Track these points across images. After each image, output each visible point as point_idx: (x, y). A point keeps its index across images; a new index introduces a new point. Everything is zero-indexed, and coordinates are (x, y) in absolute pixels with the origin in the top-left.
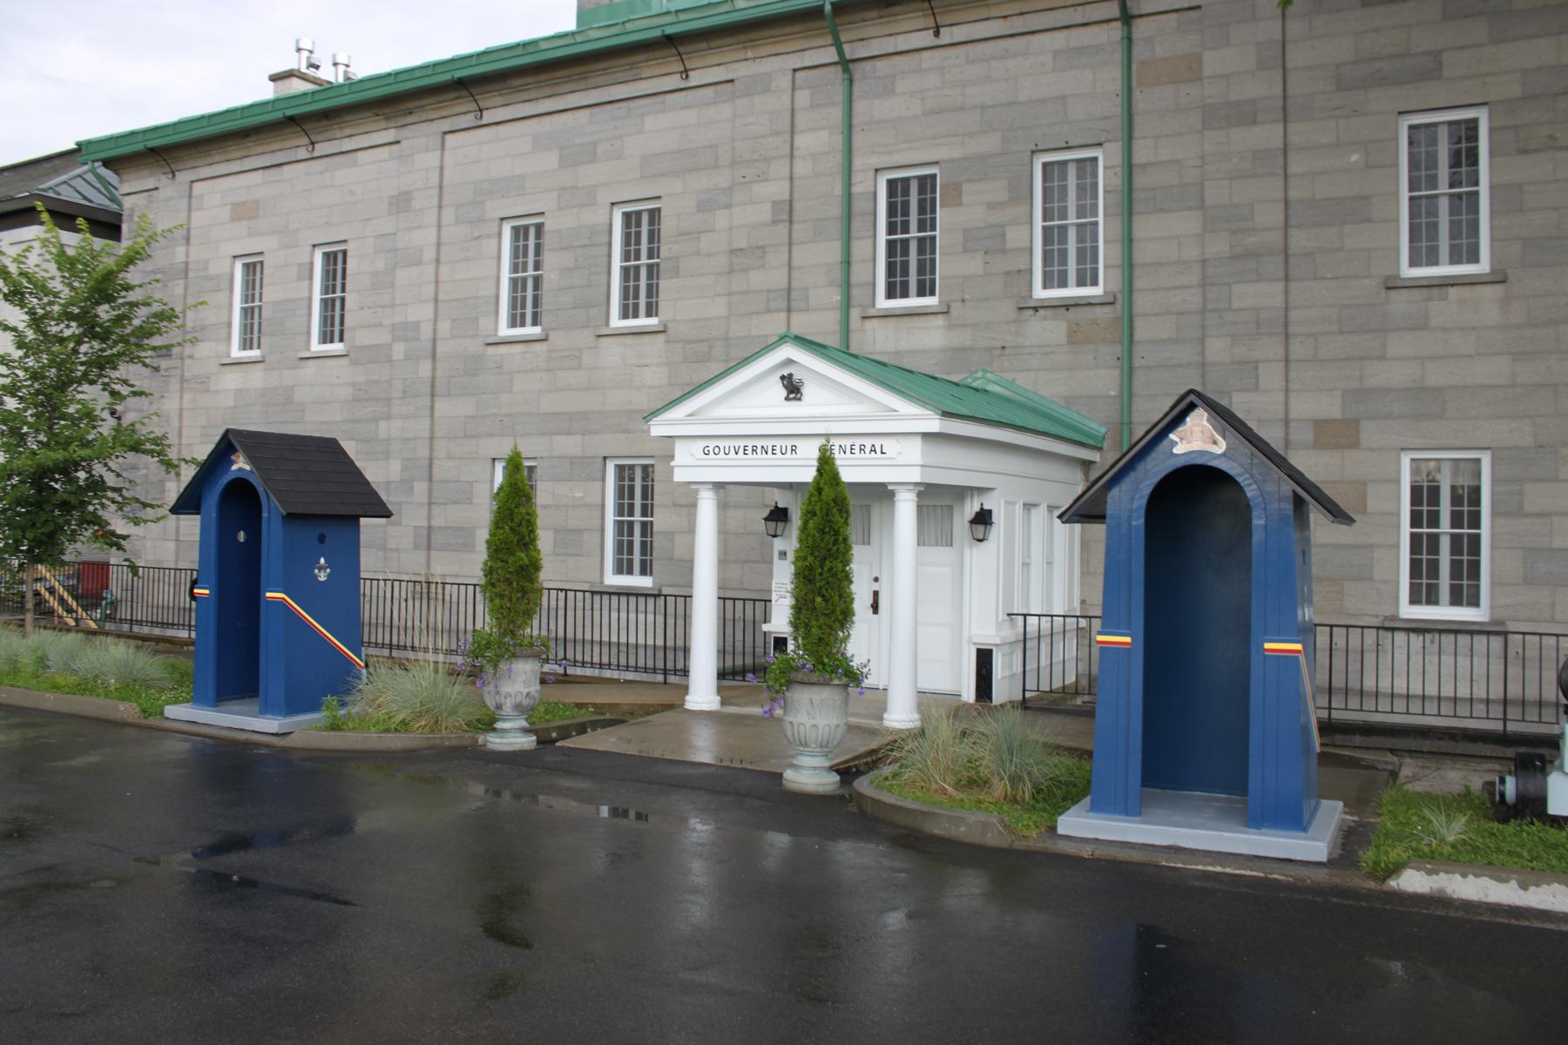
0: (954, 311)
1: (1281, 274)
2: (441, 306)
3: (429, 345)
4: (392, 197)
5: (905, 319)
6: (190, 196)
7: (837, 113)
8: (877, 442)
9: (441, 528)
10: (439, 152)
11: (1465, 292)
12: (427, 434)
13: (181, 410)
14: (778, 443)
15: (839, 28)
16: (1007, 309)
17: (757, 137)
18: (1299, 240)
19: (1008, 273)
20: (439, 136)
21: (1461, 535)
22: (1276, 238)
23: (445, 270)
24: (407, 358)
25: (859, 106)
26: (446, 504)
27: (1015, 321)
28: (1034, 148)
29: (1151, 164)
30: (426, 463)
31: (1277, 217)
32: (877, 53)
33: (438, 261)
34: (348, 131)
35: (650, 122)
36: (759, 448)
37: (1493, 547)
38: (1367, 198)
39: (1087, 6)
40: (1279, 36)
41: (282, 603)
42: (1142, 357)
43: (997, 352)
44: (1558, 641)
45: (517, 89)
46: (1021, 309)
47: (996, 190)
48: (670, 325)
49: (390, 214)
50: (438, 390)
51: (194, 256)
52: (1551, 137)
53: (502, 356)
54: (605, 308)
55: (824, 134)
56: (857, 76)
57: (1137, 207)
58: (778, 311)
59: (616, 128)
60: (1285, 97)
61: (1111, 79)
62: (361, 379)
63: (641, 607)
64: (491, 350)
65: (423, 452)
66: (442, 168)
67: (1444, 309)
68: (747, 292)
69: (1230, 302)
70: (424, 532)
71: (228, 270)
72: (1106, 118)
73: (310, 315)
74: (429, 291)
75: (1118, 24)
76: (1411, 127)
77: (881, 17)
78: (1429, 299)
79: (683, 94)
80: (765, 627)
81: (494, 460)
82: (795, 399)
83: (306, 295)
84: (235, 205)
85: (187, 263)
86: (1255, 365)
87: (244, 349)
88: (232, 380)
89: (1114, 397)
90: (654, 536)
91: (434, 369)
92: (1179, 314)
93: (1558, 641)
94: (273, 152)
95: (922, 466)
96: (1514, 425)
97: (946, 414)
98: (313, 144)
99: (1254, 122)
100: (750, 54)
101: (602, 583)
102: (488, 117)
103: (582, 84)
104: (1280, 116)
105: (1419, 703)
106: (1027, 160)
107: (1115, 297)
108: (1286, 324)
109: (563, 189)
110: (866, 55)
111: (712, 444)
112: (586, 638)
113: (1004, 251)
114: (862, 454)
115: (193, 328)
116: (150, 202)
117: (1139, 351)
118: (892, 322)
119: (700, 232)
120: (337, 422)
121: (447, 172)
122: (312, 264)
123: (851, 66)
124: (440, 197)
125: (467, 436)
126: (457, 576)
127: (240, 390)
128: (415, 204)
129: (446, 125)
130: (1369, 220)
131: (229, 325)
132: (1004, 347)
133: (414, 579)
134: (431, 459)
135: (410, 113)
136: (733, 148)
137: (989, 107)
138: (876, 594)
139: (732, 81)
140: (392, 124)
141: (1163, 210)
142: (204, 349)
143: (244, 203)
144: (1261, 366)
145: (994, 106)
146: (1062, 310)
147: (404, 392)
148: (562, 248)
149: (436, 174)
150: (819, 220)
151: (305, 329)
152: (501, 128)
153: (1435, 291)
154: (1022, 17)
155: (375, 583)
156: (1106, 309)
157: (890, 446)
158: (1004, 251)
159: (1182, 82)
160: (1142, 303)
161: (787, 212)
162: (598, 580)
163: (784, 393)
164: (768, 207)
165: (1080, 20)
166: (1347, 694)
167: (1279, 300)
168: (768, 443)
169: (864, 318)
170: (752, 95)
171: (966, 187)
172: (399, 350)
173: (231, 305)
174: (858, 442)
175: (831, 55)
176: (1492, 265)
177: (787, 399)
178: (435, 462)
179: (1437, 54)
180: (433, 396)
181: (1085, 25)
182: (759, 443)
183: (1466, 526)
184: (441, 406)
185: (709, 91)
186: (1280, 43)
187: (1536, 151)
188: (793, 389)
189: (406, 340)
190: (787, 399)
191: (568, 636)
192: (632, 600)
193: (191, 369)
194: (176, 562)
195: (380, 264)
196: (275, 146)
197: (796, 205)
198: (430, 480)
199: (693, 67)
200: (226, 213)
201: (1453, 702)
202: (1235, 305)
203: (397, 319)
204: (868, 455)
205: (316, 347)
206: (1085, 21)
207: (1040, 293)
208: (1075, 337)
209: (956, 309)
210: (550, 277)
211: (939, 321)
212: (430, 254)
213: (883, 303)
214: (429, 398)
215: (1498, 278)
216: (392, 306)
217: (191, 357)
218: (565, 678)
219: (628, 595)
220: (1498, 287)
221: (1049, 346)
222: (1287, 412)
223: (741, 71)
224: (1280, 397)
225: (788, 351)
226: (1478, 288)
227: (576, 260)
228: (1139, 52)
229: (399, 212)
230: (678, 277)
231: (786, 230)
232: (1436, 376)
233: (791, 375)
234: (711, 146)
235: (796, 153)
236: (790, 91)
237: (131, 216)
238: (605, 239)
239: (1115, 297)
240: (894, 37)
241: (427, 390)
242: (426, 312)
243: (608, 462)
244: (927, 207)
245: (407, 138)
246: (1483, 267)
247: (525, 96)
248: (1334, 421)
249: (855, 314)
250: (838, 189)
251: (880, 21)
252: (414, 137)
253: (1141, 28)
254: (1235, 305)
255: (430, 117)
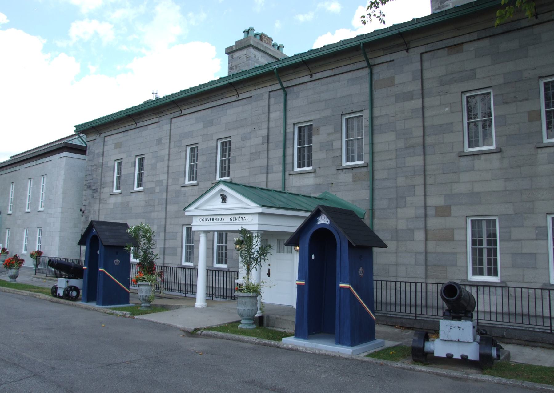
0: (317, 171)
1: (422, 153)
2: (170, 175)
3: (166, 188)
4: (157, 139)
5: (302, 175)
6: (104, 141)
7: (282, 106)
8: (246, 216)
9: (167, 248)
10: (169, 125)
11: (487, 157)
12: (164, 217)
13: (99, 209)
14: (219, 217)
15: (280, 77)
16: (333, 170)
17: (258, 115)
18: (429, 140)
19: (334, 157)
20: (170, 119)
21: (491, 249)
22: (420, 140)
23: (171, 162)
24: (159, 192)
25: (289, 102)
26: (169, 240)
27: (336, 174)
28: (342, 113)
29: (379, 116)
30: (164, 226)
31: (419, 132)
32: (294, 84)
33: (169, 160)
34: (146, 119)
35: (228, 111)
36: (214, 219)
37: (500, 253)
38: (451, 124)
39: (358, 63)
40: (420, 68)
41: (103, 271)
42: (377, 185)
43: (330, 185)
44: (422, 285)
45: (191, 103)
46: (338, 170)
47: (330, 129)
48: (233, 179)
49: (156, 145)
50: (168, 202)
51: (104, 160)
52: (515, 97)
53: (185, 190)
54: (214, 174)
55: (278, 113)
56: (288, 93)
57: (375, 132)
58: (264, 173)
59: (219, 114)
60: (422, 89)
61: (366, 87)
62: (147, 199)
63: (222, 275)
64: (183, 189)
65: (163, 223)
66: (170, 130)
67: (480, 163)
68: (255, 167)
69: (405, 164)
70: (163, 249)
71: (113, 164)
72: (364, 101)
73: (134, 178)
74: (166, 170)
75: (367, 69)
76: (467, 97)
77: (294, 72)
78: (474, 160)
79: (238, 102)
80: (236, 281)
81: (183, 225)
82: (224, 202)
83: (133, 172)
84: (116, 144)
85: (102, 163)
86: (414, 186)
87: (118, 190)
88: (113, 200)
89: (368, 199)
90: (228, 250)
91: (167, 195)
92: (389, 169)
93: (422, 285)
94: (126, 126)
95: (258, 224)
96: (506, 206)
97: (263, 206)
98: (136, 123)
99: (412, 99)
100: (256, 88)
101: (213, 266)
102: (184, 112)
103: (209, 100)
104: (421, 96)
105: (534, 319)
106: (340, 118)
107: (367, 164)
108: (425, 171)
109: (204, 135)
110: (290, 85)
111: (202, 217)
112: (216, 286)
113: (333, 150)
114: (242, 221)
115: (103, 183)
116: (94, 144)
117: (376, 183)
118: (298, 176)
119: (242, 148)
120: (140, 213)
121: (172, 131)
122: (135, 162)
123: (286, 90)
124: (170, 139)
125: (176, 217)
126: (172, 264)
127: (115, 203)
128: (163, 142)
129: (172, 116)
130: (452, 132)
131: (113, 182)
132: (332, 183)
133: (438, 281)
134: (165, 225)
135: (162, 112)
136: (251, 119)
137: (328, 100)
138: (269, 270)
139: (251, 97)
140: (157, 116)
141: (383, 132)
142: (106, 190)
143: (118, 143)
144: (416, 187)
145: (330, 100)
146: (351, 169)
147: (158, 203)
148: (203, 155)
149: (168, 132)
150: (276, 142)
151: (133, 183)
152: (187, 116)
153: (476, 157)
154: (337, 69)
155: (531, 291)
156: (365, 169)
157: (250, 217)
158: (333, 150)
159: (388, 87)
160: (377, 166)
161: (268, 139)
162: (211, 265)
163: (221, 200)
164: (261, 138)
165: (356, 68)
166: (422, 307)
167: (422, 163)
168: (217, 217)
169: (290, 175)
170: (257, 101)
171: (321, 129)
172: (157, 190)
173: (114, 176)
174: (241, 216)
175: (279, 86)
176: (496, 146)
177: (222, 202)
178: (167, 226)
179: (473, 70)
180: (166, 204)
181: (357, 70)
182: (214, 217)
183: (477, 245)
184: (169, 207)
185: (245, 101)
186: (420, 70)
187: (510, 103)
188: (224, 199)
189: (159, 186)
190: (222, 202)
191: (213, 286)
192: (487, 289)
193: (103, 196)
194: (426, 277)
195: (153, 161)
196: (127, 125)
197: (270, 137)
198: (165, 232)
199: (240, 93)
200: (113, 146)
201: (495, 314)
202: (407, 165)
203: (157, 179)
204: (243, 221)
205: (136, 189)
206: (357, 68)
207: (345, 164)
208: (355, 179)
209: (317, 170)
210: (200, 164)
211: (312, 175)
212: (166, 158)
213: (296, 169)
214: (165, 205)
215: (498, 151)
216: (156, 175)
217: (103, 192)
218: (185, 298)
219: (221, 271)
220: (499, 154)
221: (347, 182)
222: (425, 203)
223: (254, 93)
224: (422, 198)
225: (222, 187)
226: (492, 155)
227: (207, 158)
228: (375, 77)
229: (158, 144)
230: (235, 163)
231: (266, 146)
232: (478, 188)
233: (223, 194)
234: (246, 119)
235: (270, 120)
236: (268, 99)
237: (89, 148)
238: (215, 151)
239: (367, 164)
240: (299, 78)
241: (164, 202)
242: (164, 177)
243: (184, 226)
244: (310, 136)
245: (161, 121)
246: (493, 147)
247: (194, 105)
248: (442, 206)
249: (287, 173)
250: (282, 131)
251: (294, 73)
252: (163, 120)
253: (376, 70)
254: (407, 165)
255: (168, 114)
